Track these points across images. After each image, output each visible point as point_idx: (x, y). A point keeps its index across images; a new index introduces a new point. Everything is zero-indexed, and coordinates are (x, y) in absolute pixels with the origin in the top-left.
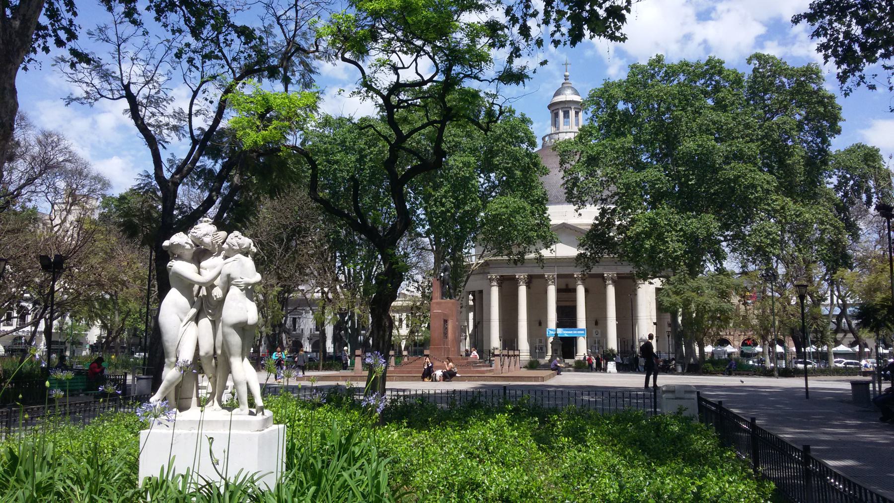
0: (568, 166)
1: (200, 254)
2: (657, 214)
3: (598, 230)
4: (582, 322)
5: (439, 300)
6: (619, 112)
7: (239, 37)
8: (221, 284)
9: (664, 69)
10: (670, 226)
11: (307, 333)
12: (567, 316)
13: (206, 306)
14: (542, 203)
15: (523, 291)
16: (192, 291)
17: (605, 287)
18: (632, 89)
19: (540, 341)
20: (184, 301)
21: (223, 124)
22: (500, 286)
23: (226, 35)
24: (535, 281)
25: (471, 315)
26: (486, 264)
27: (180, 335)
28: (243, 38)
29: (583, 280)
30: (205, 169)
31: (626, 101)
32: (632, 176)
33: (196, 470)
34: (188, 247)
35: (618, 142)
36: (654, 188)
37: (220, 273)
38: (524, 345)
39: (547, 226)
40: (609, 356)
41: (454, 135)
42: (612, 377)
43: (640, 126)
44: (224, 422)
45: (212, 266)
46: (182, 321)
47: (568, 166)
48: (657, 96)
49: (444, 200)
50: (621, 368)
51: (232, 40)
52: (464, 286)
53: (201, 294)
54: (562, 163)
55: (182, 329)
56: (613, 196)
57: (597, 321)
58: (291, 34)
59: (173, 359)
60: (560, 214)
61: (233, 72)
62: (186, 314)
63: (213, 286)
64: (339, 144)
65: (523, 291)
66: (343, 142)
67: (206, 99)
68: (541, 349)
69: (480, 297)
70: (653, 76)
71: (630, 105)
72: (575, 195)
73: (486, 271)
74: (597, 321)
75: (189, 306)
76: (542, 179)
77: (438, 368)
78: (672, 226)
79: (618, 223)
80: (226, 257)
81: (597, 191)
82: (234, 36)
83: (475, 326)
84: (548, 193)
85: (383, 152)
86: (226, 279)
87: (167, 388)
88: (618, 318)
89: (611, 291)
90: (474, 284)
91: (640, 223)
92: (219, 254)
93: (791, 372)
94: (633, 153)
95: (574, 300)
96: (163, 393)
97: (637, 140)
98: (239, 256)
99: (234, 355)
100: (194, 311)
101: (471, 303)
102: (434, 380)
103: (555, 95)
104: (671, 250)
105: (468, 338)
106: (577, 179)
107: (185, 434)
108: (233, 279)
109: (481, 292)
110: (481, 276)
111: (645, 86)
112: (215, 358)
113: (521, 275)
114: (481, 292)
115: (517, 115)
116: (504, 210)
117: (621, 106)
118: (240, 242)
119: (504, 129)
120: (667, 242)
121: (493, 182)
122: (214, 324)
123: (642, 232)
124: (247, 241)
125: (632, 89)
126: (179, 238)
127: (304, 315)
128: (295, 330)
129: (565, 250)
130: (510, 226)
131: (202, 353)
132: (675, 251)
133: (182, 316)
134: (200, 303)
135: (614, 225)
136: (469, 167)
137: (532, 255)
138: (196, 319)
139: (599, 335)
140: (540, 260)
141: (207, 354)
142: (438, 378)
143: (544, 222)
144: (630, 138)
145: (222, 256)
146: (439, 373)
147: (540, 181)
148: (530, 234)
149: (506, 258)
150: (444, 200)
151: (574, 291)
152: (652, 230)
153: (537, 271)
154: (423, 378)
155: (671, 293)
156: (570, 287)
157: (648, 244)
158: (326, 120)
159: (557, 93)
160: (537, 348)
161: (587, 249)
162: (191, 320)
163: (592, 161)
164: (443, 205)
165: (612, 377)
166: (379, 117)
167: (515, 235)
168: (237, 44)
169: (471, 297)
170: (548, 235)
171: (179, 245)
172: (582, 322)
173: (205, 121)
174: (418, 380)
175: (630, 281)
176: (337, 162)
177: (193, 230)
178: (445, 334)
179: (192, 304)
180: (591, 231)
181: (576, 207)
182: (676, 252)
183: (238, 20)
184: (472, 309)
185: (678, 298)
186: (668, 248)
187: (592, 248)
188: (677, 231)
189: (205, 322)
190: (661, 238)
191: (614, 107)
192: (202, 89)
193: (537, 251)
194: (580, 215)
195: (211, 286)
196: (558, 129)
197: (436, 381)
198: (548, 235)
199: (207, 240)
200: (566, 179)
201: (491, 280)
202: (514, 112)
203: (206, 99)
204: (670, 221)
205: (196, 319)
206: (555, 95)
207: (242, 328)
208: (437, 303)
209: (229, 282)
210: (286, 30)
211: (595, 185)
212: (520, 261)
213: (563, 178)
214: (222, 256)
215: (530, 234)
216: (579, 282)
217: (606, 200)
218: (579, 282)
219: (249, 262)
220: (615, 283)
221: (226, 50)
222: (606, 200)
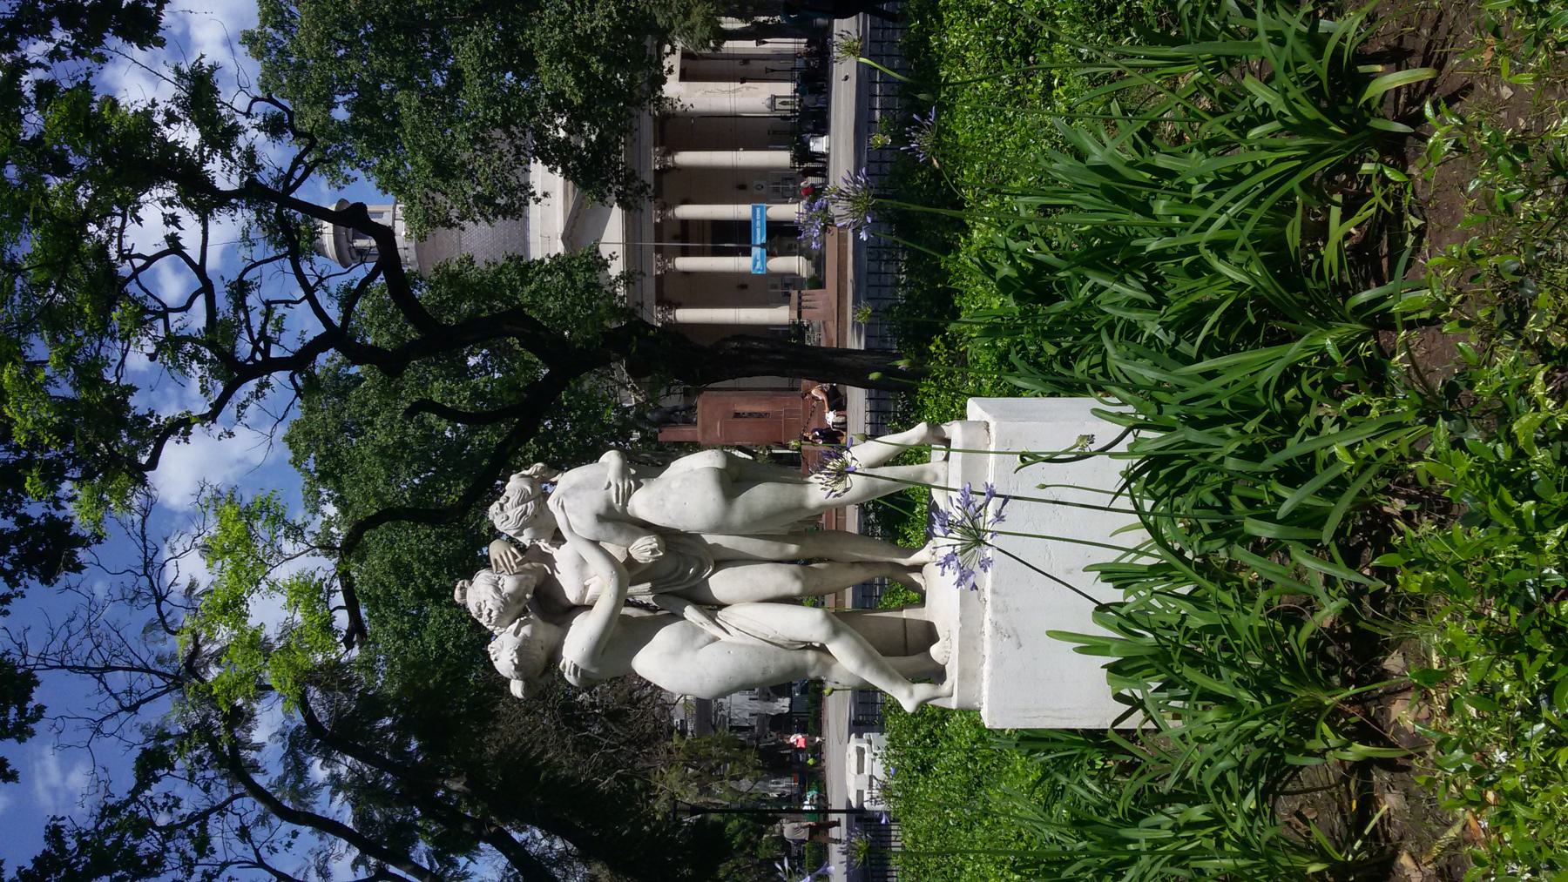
0: (454, 214)
1: (547, 604)
2: (543, 46)
3: (575, 168)
4: (742, 211)
5: (698, 429)
6: (352, 119)
7: (157, 780)
8: (622, 539)
9: (270, 30)
10: (564, 22)
11: (758, 707)
12: (731, 237)
13: (676, 577)
16: (640, 619)
18: (308, 92)
19: (775, 287)
20: (665, 637)
21: (347, 818)
23: (155, 806)
27: (751, 641)
28: (160, 772)
29: (666, 206)
30: (435, 853)
31: (332, 105)
32: (471, 97)
33: (1104, 500)
34: (525, 630)
35: (409, 117)
37: (595, 543)
39: (570, 258)
40: (803, 154)
42: (837, 145)
43: (379, 76)
44: (965, 463)
45: (585, 573)
46: (715, 639)
47: (454, 214)
48: (320, 43)
50: (822, 128)
51: (167, 796)
53: (648, 599)
54: (449, 224)
55: (736, 637)
56: (511, 135)
57: (738, 185)
58: (159, 682)
59: (810, 656)
60: (546, 227)
61: (235, 797)
62: (697, 631)
63: (630, 562)
64: (406, 644)
66: (401, 634)
67: (289, 845)
70: (283, 52)
71: (339, 98)
72: (511, 203)
74: (738, 185)
75: (678, 624)
76: (480, 263)
77: (823, 419)
79: (562, 134)
80: (558, 538)
81: (500, 159)
82: (155, 791)
85: (421, 552)
86: (609, 526)
87: (882, 670)
89: (686, 158)
92: (549, 559)
94: (430, 99)
95: (701, 223)
96: (892, 678)
97: (405, 84)
98: (551, 503)
99: (803, 498)
100: (690, 612)
102: (843, 426)
104: (607, 23)
106: (478, 197)
107: (996, 611)
108: (610, 507)
111: (301, 67)
112: (808, 562)
117: (341, 114)
118: (514, 499)
119: (380, 326)
120: (593, 29)
121: (485, 356)
122: (725, 560)
123: (575, 76)
124: (515, 485)
125: (308, 92)
126: (504, 653)
127: (725, 713)
128: (752, 728)
130: (565, 317)
131: (795, 588)
132: (609, 16)
133: (701, 639)
134: (672, 599)
135: (567, 140)
137: (621, 291)
138: (711, 607)
140: (628, 277)
141: (797, 577)
142: (841, 419)
143: (559, 263)
144: (400, 97)
145: (553, 550)
146: (831, 417)
147: (484, 267)
148: (580, 285)
151: (685, 223)
152: (571, 58)
155: (688, 23)
156: (677, 230)
157: (597, 67)
161: (610, 190)
162: (712, 619)
163: (444, 169)
165: (837, 145)
168: (167, 785)
170: (581, 259)
171: (521, 651)
172: (742, 211)
173: (339, 857)
176: (441, 644)
177: (483, 621)
178: (760, 415)
179: (676, 616)
180: (576, 181)
181: (532, 202)
182: (610, 13)
183: (125, 781)
185: (696, 10)
186: (603, 28)
187: (608, 181)
188: (573, 12)
189: (721, 584)
190: (586, 42)
191: (342, 127)
192: (159, 668)
194: (545, 195)
195: (629, 571)
198: (581, 259)
199: (509, 584)
200: (478, 217)
203: (289, 845)
204: (554, 24)
205: (711, 607)
207: (732, 481)
208: (704, 431)
209: (616, 518)
210: (154, 692)
211: (489, 162)
213: (476, 222)
214: (553, 550)
215: (580, 285)
216: (670, 214)
217: (518, 148)
218: (670, 214)
219: (567, 480)
221: (186, 809)
222: (518, 148)
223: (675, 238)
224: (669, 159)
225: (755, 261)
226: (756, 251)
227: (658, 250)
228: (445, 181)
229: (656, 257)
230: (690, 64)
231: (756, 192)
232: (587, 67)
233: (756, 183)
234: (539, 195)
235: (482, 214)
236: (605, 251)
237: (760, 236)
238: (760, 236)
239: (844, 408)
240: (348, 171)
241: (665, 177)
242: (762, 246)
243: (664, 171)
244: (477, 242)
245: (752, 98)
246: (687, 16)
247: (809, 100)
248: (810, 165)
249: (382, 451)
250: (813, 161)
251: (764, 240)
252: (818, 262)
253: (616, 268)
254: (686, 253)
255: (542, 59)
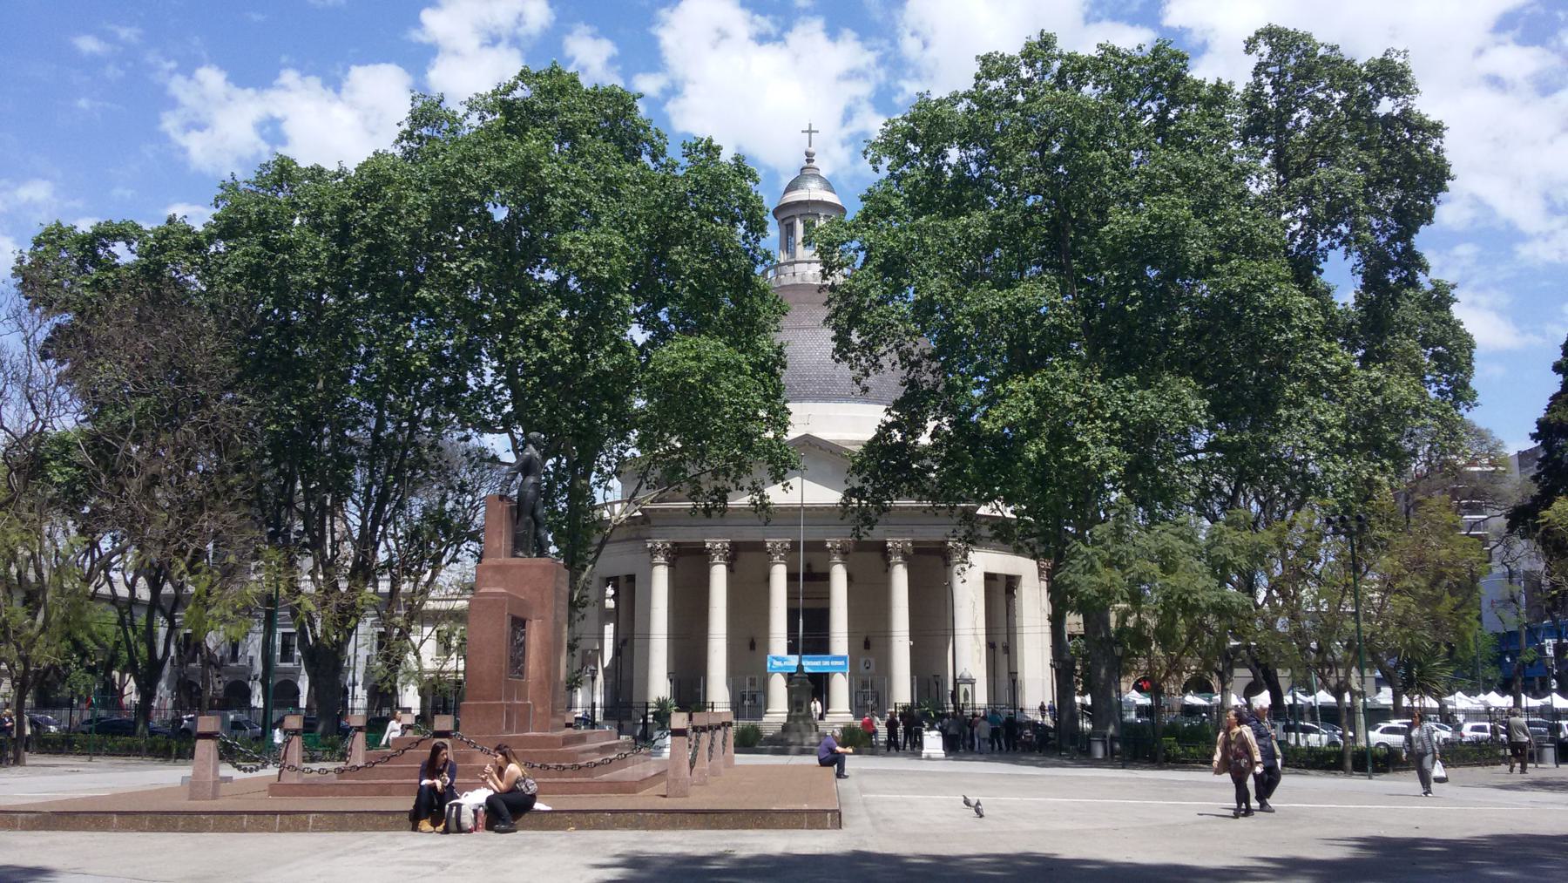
4: (840, 640)
12: (810, 631)
14: (773, 373)
15: (719, 576)
17: (887, 569)
19: (753, 682)
22: (672, 565)
24: (745, 557)
25: (609, 630)
26: (647, 518)
29: (845, 554)
36: (1042, 326)
38: (719, 692)
41: (577, 183)
49: (545, 333)
52: (593, 562)
65: (719, 576)
68: (754, 698)
69: (630, 588)
73: (643, 534)
78: (1091, 410)
83: (617, 651)
84: (786, 350)
88: (914, 634)
89: (900, 577)
90: (614, 560)
91: (1012, 402)
93: (1376, 759)
95: (826, 596)
101: (610, 604)
103: (788, 190)
105: (600, 677)
109: (631, 579)
110: (630, 545)
113: (717, 543)
114: (631, 579)
115: (726, 156)
116: (693, 363)
120: (1083, 444)
128: (234, 657)
129: (809, 492)
130: (706, 404)
136: (609, 255)
139: (872, 669)
140: (763, 509)
142: (467, 819)
146: (473, 799)
149: (689, 505)
150: (545, 333)
151: (826, 577)
153: (750, 534)
154: (413, 820)
155: (1098, 564)
156: (817, 569)
158: (283, 168)
159: (792, 187)
160: (749, 697)
161: (866, 480)
164: (543, 345)
166: (398, 152)
167: (716, 431)
169: (610, 591)
174: (396, 827)
175: (938, 560)
178: (517, 662)
184: (613, 615)
185: (1116, 573)
187: (876, 479)
188: (1104, 420)
190: (1060, 437)
193: (756, 489)
196: (793, 254)
197: (460, 829)
201: (653, 552)
202: (717, 150)
206: (788, 190)
212: (716, 508)
213: (828, 303)
220: (910, 561)
223: (808, 566)
224: (899, 559)
225: (783, 660)
226: (794, 660)
227: (795, 546)
228: (881, 267)
229: (787, 542)
230: (1001, 587)
231: (862, 661)
232: (1031, 436)
233: (872, 660)
234: (865, 381)
235: (838, 310)
236: (795, 481)
237: (812, 664)
238: (812, 664)
239: (490, 827)
240: (887, 161)
241: (876, 556)
242: (800, 667)
243: (882, 550)
244: (807, 342)
245: (969, 655)
246: (1109, 564)
247: (984, 729)
248: (901, 728)
249: (530, 165)
250: (907, 732)
251: (807, 670)
252: (779, 744)
253: (776, 495)
254: (792, 577)
255: (1038, 381)
